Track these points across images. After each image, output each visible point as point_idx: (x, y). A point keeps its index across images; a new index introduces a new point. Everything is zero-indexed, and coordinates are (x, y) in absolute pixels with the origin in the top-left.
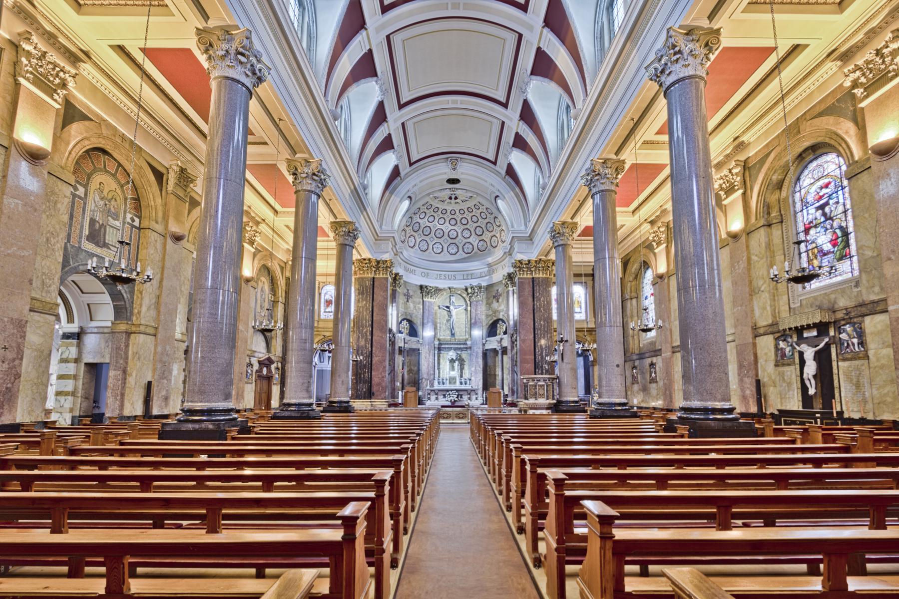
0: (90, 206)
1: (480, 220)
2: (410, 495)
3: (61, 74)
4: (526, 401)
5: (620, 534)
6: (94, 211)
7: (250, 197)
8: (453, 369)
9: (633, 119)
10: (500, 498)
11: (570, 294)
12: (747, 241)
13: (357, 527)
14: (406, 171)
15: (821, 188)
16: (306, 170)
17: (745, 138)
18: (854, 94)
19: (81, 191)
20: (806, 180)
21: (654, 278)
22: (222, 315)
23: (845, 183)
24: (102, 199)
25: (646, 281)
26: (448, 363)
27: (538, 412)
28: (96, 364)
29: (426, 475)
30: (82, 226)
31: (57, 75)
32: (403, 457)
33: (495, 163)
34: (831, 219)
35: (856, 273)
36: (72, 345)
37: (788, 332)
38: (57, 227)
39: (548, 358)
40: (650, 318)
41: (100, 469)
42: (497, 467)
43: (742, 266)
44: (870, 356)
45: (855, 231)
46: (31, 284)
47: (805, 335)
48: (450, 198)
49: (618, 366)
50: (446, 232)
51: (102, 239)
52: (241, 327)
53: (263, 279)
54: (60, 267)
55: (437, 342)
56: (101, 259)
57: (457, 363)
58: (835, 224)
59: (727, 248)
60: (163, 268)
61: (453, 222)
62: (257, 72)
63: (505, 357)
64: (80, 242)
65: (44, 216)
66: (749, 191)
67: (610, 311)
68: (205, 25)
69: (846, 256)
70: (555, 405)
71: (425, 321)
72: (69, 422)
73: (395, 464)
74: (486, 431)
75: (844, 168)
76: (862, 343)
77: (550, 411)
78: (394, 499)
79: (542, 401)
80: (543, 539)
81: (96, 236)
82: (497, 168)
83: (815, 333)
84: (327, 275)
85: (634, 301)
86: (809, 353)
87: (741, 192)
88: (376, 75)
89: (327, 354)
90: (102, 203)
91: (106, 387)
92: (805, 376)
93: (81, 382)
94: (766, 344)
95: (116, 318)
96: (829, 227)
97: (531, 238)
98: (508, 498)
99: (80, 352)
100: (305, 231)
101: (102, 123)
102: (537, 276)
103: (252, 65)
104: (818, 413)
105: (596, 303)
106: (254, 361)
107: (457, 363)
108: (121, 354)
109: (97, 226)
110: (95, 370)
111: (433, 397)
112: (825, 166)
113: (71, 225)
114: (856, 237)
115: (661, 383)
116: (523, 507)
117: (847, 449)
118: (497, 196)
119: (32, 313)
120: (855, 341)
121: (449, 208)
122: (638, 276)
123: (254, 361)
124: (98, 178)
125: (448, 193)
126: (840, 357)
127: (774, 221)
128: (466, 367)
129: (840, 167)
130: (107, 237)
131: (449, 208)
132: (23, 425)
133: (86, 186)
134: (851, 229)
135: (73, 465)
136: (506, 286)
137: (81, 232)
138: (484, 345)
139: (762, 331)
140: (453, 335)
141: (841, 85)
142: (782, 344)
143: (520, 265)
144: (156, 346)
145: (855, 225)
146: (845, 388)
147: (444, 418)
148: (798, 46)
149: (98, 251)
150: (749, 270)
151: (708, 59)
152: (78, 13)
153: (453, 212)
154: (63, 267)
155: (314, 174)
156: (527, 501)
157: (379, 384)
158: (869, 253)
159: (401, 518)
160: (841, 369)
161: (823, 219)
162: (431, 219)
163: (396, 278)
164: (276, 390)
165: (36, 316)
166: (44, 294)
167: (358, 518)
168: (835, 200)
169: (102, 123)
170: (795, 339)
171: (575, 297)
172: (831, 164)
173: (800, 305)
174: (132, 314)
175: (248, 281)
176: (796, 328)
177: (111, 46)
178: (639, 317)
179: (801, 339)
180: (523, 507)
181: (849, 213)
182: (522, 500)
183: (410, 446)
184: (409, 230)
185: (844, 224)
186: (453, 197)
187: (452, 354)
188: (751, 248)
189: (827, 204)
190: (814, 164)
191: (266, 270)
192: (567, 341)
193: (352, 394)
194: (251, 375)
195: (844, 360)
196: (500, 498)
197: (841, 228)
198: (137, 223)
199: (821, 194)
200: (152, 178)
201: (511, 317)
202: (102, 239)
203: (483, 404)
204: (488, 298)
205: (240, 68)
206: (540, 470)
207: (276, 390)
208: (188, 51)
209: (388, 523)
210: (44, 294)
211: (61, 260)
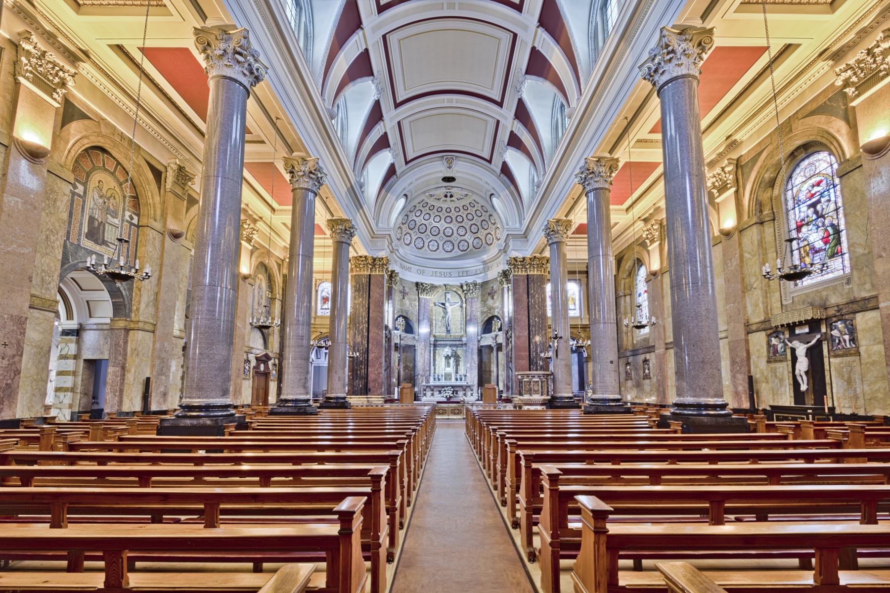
0: (90, 203)
1: (476, 217)
2: (405, 490)
3: (61, 73)
4: (521, 397)
5: (614, 529)
6: (93, 209)
7: (247, 196)
8: (448, 365)
9: (626, 118)
10: (495, 493)
11: (564, 291)
12: (740, 239)
13: (354, 522)
14: (402, 170)
15: (813, 186)
16: (303, 168)
17: (737, 137)
18: (845, 93)
19: (80, 189)
20: (798, 179)
21: (647, 275)
22: (220, 312)
23: (837, 181)
24: (101, 197)
25: (639, 278)
26: (443, 359)
27: (532, 408)
28: (95, 361)
29: (422, 470)
30: (81, 224)
31: (57, 75)
32: (399, 452)
33: (490, 162)
34: (823, 216)
35: (848, 270)
36: (72, 342)
37: (780, 329)
38: (57, 224)
39: (542, 355)
40: (644, 315)
41: (99, 464)
42: (492, 463)
43: (735, 264)
44: (862, 352)
45: (847, 229)
46: (31, 281)
47: (797, 332)
48: (446, 196)
49: (612, 362)
50: (442, 230)
51: (101, 237)
52: (239, 324)
53: (260, 276)
54: (59, 264)
55: (432, 339)
56: (100, 256)
57: (452, 359)
58: (827, 222)
59: (720, 246)
60: (161, 265)
61: (448, 220)
62: (255, 71)
63: (500, 353)
64: (79, 240)
65: (43, 214)
66: (741, 189)
67: (604, 308)
68: (203, 25)
69: (837, 253)
70: (549, 401)
71: (421, 318)
72: (68, 417)
73: (391, 459)
74: (481, 427)
75: (836, 166)
76: (853, 340)
77: (544, 407)
78: (390, 494)
79: (537, 397)
80: (537, 534)
81: (95, 233)
82: (492, 166)
83: (807, 330)
84: (324, 272)
85: (628, 298)
86: (801, 349)
87: (733, 190)
88: (372, 74)
89: (324, 350)
90: (101, 201)
91: (105, 383)
92: (797, 372)
93: (80, 378)
94: (759, 341)
95: (115, 315)
96: (820, 224)
97: (525, 236)
98: (503, 493)
99: (79, 349)
100: (302, 228)
101: (101, 121)
102: (532, 273)
103: (250, 65)
104: (810, 408)
105: (590, 300)
106: (252, 357)
107: (452, 359)
108: (120, 350)
109: (96, 223)
110: (94, 366)
111: (429, 393)
112: (817, 164)
113: (70, 223)
114: (848, 235)
115: (654, 380)
116: (518, 502)
117: (838, 445)
118: (492, 194)
119: (32, 310)
120: (847, 337)
121: (445, 206)
122: (632, 274)
123: (252, 357)
124: (97, 176)
125: (444, 191)
126: (832, 354)
127: (767, 219)
128: (461, 364)
129: (831, 165)
130: (106, 235)
131: (445, 206)
132: (23, 421)
133: (85, 184)
134: (842, 227)
135: (72, 460)
136: (501, 283)
137: (80, 229)
138: (479, 341)
139: (754, 328)
140: (448, 331)
141: (833, 84)
142: (774, 341)
143: (514, 263)
144: (154, 342)
145: (846, 223)
146: (837, 384)
147: (440, 414)
148: (790, 45)
149: (97, 248)
150: (742, 267)
151: (701, 59)
152: (77, 13)
153: (448, 210)
154: (63, 264)
155: (311, 172)
156: (522, 496)
157: (375, 381)
158: (860, 251)
159: (397, 513)
160: (833, 365)
161: (815, 217)
162: (427, 217)
163: (392, 275)
164: (273, 386)
165: (36, 313)
166: (44, 291)
167: (354, 513)
168: (827, 198)
169: (101, 121)
170: (787, 336)
171: (570, 294)
172: (823, 163)
173: (792, 302)
174: (130, 310)
175: (245, 278)
176: (788, 325)
177: (110, 46)
178: (633, 314)
179: (793, 336)
180: (518, 502)
181: (841, 211)
182: (517, 495)
183: (406, 441)
184: (405, 228)
185: (835, 222)
186: (449, 195)
187: (448, 351)
188: (743, 245)
189: (819, 202)
190: (806, 162)
191: (263, 267)
192: (561, 338)
193: (349, 390)
194: (249, 371)
195: (836, 356)
196: (495, 493)
197: (832, 225)
198: (135, 221)
199: (813, 192)
200: (150, 176)
201: (506, 314)
202: (101, 237)
203: (478, 400)
204: (483, 295)
205: (237, 68)
206: (534, 466)
207: (273, 386)
208: (186, 51)
209: (384, 518)
210: (44, 291)
211: (60, 257)
